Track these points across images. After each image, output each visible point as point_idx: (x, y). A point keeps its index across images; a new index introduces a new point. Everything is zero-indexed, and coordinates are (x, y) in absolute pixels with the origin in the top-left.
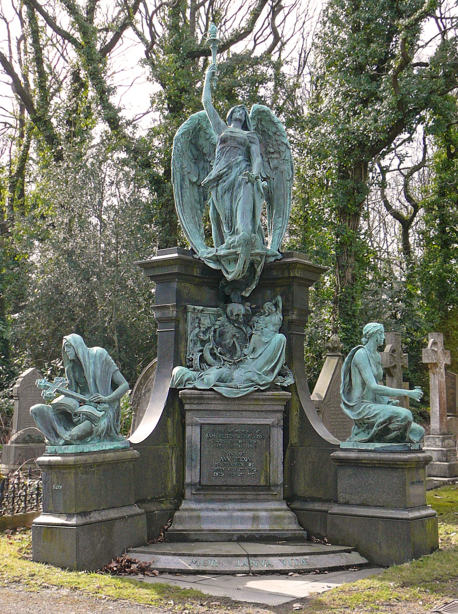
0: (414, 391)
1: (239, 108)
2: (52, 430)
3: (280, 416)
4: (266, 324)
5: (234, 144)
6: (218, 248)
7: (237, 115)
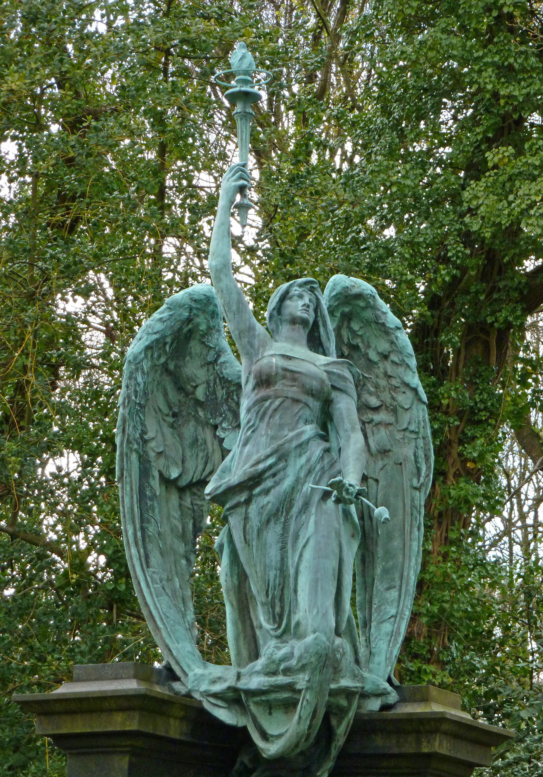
1: (300, 286)
5: (293, 392)
6: (243, 671)
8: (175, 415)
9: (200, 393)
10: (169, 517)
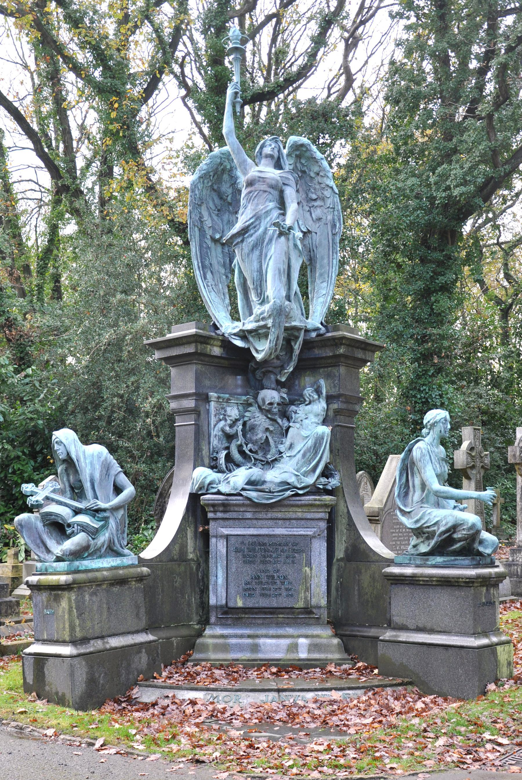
0: (486, 492)
2: (41, 545)
3: (323, 525)
4: (306, 415)
5: (264, 187)
6: (245, 322)
7: (267, 150)
8: (219, 210)
9: (229, 199)
10: (217, 256)
